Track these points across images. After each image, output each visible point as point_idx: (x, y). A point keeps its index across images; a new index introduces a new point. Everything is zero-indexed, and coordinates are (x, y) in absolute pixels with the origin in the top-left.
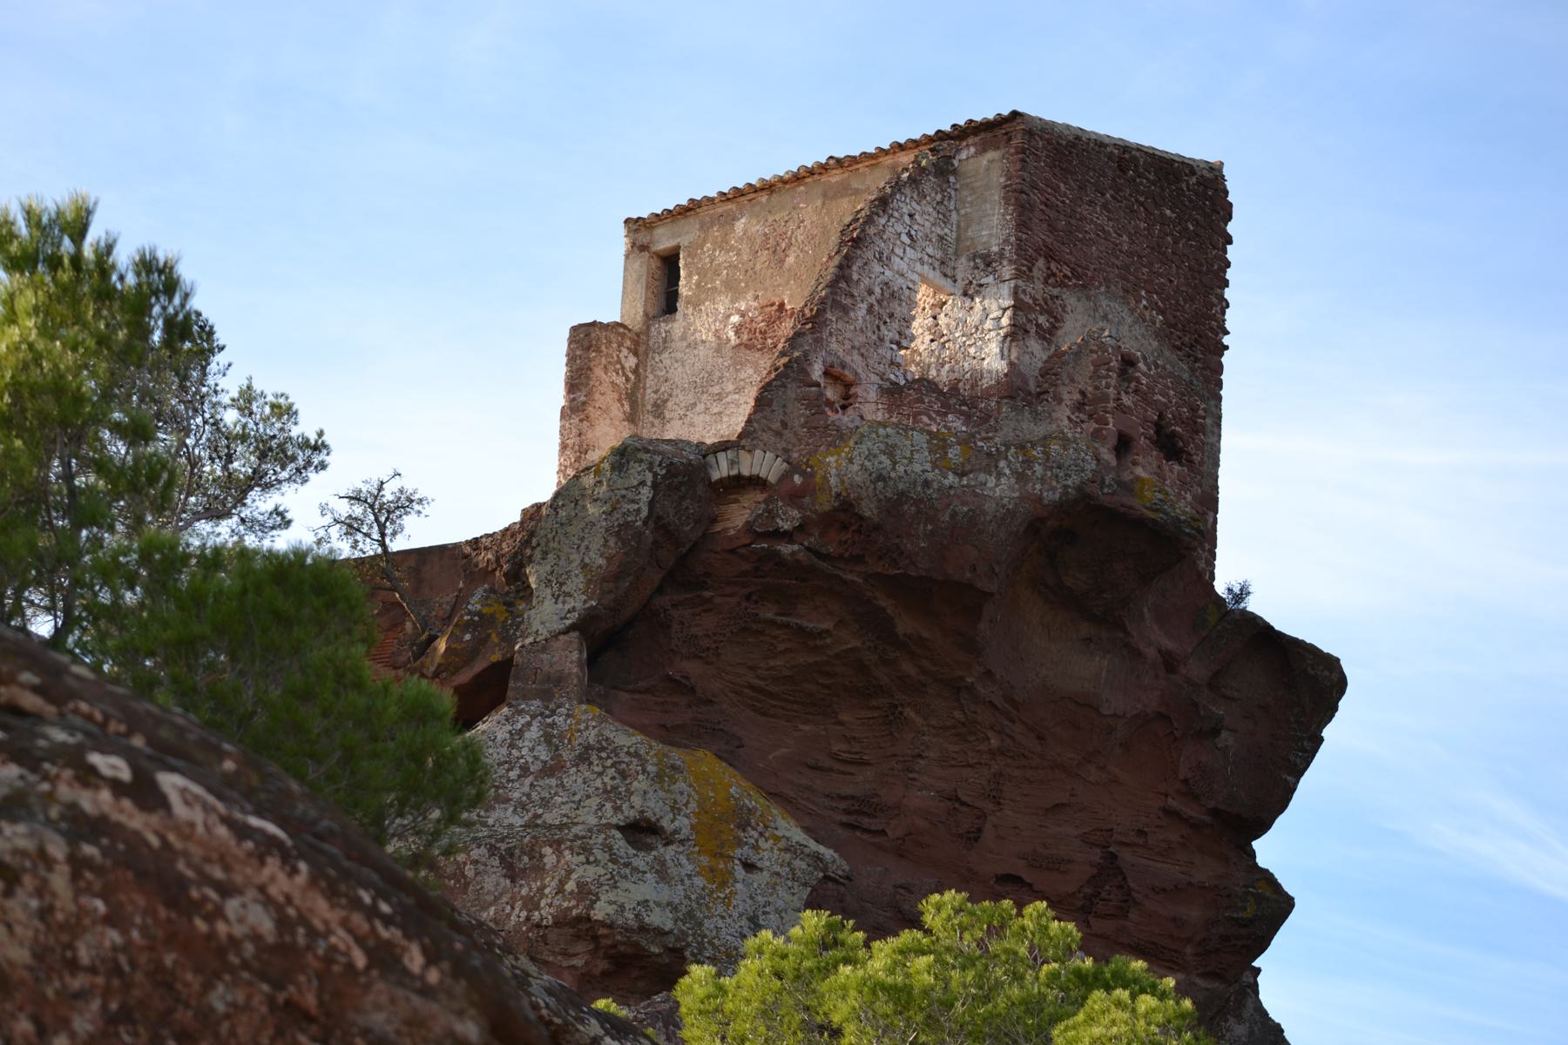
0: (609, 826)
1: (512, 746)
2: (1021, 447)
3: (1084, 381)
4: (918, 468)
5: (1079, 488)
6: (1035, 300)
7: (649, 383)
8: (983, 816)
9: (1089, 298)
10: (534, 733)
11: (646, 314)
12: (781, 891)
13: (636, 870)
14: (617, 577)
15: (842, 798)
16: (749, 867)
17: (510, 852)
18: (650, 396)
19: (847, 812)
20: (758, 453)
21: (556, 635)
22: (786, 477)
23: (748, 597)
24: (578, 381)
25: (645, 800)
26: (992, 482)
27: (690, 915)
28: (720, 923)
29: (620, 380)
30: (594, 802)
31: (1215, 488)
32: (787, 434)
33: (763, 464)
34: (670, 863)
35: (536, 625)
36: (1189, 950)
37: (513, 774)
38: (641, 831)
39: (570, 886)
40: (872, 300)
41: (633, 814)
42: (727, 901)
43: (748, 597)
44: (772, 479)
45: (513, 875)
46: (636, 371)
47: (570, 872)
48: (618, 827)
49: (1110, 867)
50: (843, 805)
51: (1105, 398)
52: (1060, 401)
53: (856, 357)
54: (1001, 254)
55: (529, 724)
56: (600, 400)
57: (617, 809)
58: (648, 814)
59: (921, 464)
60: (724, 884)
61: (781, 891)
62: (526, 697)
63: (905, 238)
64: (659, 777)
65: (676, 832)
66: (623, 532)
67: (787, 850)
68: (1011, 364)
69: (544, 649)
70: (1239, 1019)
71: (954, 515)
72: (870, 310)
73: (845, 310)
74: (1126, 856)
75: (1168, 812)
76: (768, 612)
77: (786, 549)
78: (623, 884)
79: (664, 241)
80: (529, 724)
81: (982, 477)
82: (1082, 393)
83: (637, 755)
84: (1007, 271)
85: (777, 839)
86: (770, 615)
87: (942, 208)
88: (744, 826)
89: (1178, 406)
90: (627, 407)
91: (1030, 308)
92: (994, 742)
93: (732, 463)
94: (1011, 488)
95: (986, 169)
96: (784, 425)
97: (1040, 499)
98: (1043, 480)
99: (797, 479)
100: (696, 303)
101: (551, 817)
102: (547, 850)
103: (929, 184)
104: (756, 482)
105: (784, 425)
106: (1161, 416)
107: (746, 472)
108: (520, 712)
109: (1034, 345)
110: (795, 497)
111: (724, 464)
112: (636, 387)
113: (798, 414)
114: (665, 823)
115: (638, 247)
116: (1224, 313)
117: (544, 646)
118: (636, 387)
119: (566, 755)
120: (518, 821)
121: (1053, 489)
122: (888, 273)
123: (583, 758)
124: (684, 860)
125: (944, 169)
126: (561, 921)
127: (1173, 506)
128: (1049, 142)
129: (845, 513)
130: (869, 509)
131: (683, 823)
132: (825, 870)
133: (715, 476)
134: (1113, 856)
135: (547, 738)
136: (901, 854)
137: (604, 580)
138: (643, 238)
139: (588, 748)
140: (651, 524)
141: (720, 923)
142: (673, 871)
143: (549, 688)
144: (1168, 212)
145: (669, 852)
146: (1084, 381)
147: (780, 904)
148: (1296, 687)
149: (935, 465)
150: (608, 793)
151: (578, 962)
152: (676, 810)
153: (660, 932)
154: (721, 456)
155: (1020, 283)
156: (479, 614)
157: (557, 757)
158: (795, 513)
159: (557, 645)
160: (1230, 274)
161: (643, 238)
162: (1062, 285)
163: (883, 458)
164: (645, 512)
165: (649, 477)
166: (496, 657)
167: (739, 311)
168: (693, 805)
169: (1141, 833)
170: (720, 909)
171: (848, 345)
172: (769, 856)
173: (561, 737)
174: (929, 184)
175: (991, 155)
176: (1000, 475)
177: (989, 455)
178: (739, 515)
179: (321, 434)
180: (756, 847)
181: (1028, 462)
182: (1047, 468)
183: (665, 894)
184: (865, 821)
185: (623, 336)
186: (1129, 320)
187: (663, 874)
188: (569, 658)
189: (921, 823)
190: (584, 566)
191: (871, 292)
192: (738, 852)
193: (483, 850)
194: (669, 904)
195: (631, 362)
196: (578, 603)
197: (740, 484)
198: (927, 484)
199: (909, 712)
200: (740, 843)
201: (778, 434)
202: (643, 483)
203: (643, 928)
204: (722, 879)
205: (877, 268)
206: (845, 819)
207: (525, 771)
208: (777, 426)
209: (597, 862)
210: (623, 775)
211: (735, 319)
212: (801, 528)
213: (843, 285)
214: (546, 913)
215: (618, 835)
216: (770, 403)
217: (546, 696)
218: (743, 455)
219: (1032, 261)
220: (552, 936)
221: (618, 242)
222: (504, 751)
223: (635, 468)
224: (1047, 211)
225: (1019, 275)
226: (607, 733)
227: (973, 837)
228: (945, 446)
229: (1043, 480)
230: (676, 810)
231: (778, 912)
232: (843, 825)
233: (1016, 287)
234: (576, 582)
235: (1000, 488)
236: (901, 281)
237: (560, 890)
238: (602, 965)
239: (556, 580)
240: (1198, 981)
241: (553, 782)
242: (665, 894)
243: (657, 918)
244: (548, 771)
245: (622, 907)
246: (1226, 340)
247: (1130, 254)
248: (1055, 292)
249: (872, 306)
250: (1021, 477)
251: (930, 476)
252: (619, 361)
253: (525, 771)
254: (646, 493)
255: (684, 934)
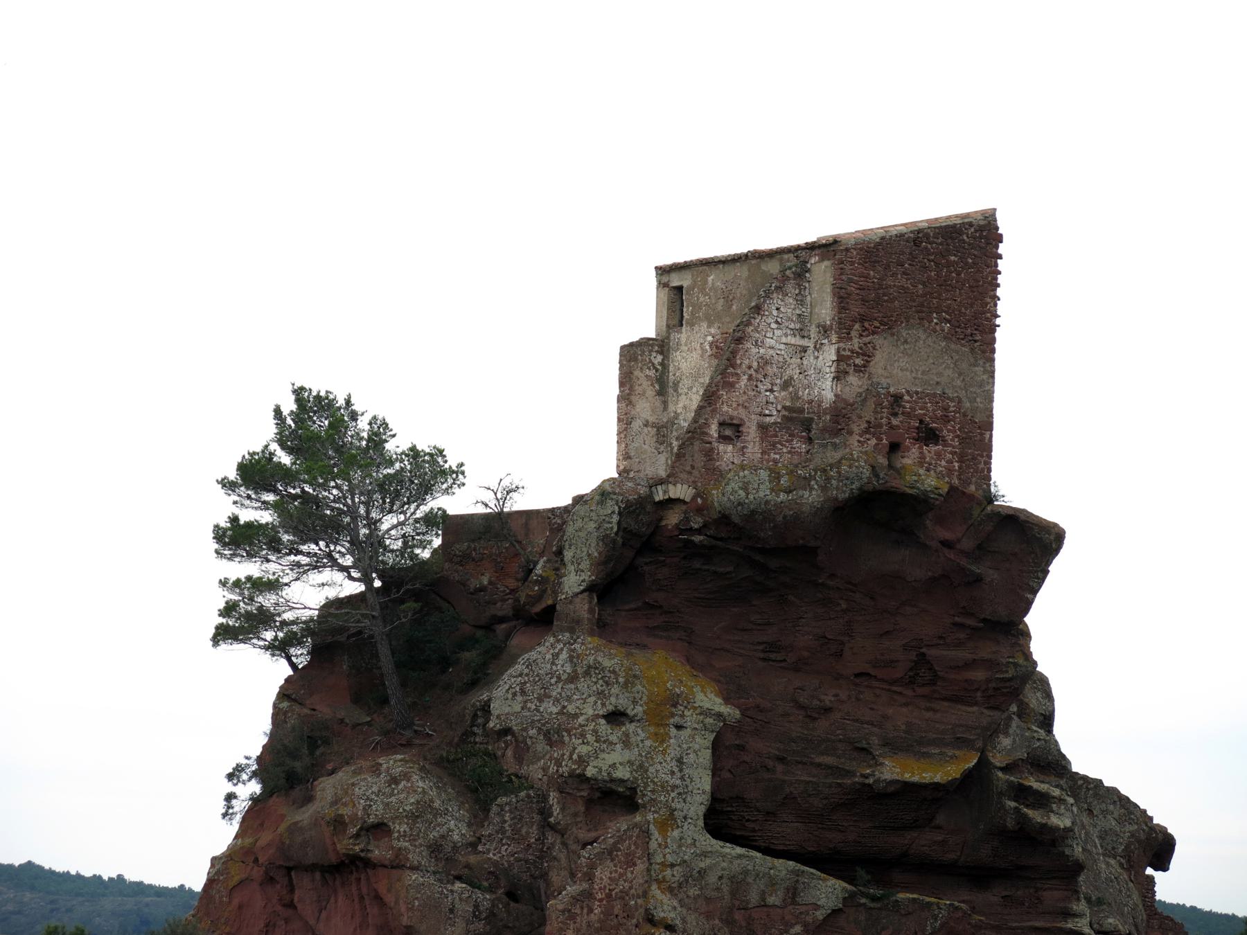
0: (597, 716)
1: (553, 663)
2: (824, 471)
3: (868, 414)
4: (761, 494)
5: (859, 489)
6: (852, 351)
7: (671, 369)
8: (843, 643)
9: (893, 335)
10: (564, 655)
11: (668, 326)
12: (698, 739)
13: (611, 743)
14: (605, 563)
15: (759, 643)
16: (679, 727)
17: (548, 732)
18: (671, 377)
19: (763, 651)
20: (679, 486)
21: (577, 595)
22: (694, 498)
23: (685, 558)
24: (626, 380)
25: (618, 699)
26: (806, 494)
27: (641, 766)
28: (659, 767)
29: (652, 373)
30: (592, 699)
31: (991, 416)
32: (695, 472)
33: (680, 491)
34: (631, 735)
35: (566, 589)
36: (979, 694)
37: (553, 681)
38: (616, 717)
39: (575, 757)
40: (752, 372)
41: (611, 708)
42: (664, 752)
43: (685, 558)
44: (687, 499)
45: (551, 743)
46: (662, 364)
47: (575, 749)
48: (604, 717)
49: (922, 659)
50: (761, 647)
51: (880, 426)
52: (850, 433)
53: (741, 410)
54: (831, 325)
55: (562, 649)
56: (638, 389)
57: (603, 705)
58: (620, 707)
59: (764, 492)
60: (663, 741)
61: (698, 739)
62: (562, 630)
63: (774, 326)
64: (626, 683)
65: (635, 715)
66: (604, 538)
67: (701, 714)
68: (836, 396)
69: (571, 602)
70: (1007, 734)
71: (785, 517)
72: (750, 378)
73: (732, 385)
74: (932, 653)
75: (955, 624)
76: (697, 564)
77: (697, 538)
78: (602, 756)
79: (684, 280)
80: (562, 649)
81: (801, 493)
82: (868, 422)
83: (614, 672)
84: (834, 338)
85: (695, 708)
86: (698, 566)
87: (799, 298)
88: (675, 706)
89: (934, 411)
90: (657, 387)
91: (849, 357)
92: (844, 606)
93: (665, 492)
94: (818, 496)
95: (822, 272)
96: (693, 467)
97: (836, 499)
98: (837, 488)
99: (699, 500)
100: (691, 324)
101: (571, 709)
102: (565, 734)
103: (791, 287)
104: (678, 501)
105: (693, 467)
106: (921, 422)
107: (672, 496)
108: (558, 641)
109: (853, 379)
110: (699, 510)
111: (661, 493)
112: (663, 373)
113: (699, 460)
114: (629, 711)
115: (662, 285)
116: (996, 305)
117: (570, 601)
118: (663, 373)
119: (580, 670)
120: (555, 710)
121: (844, 492)
122: (762, 351)
123: (587, 673)
124: (640, 731)
125: (801, 273)
126: (572, 774)
127: (923, 484)
128: (861, 249)
129: (724, 519)
130: (736, 519)
131: (639, 709)
132: (724, 720)
133: (657, 499)
134: (924, 654)
135: (571, 658)
136: (797, 670)
137: (599, 564)
138: (665, 279)
139: (589, 667)
140: (621, 533)
141: (659, 767)
142: (633, 740)
143: (573, 626)
144: (953, 258)
145: (631, 727)
146: (868, 414)
147: (697, 747)
148: (1031, 545)
149: (772, 490)
150: (600, 694)
151: (585, 794)
152: (635, 702)
153: (622, 781)
154: (659, 487)
155: (841, 345)
156: (540, 576)
157: (575, 671)
158: (700, 520)
159: (577, 600)
160: (1000, 279)
161: (665, 279)
162: (874, 333)
163: (741, 492)
164: (615, 529)
165: (616, 508)
166: (550, 602)
167: (711, 334)
168: (645, 698)
169: (941, 638)
170: (660, 758)
171: (734, 405)
172: (691, 718)
173: (578, 657)
174: (791, 287)
175: (826, 263)
176: (812, 489)
177: (805, 478)
178: (673, 519)
179: (462, 465)
180: (682, 716)
181: (828, 479)
182: (839, 481)
183: (627, 755)
184: (773, 656)
185: (652, 345)
186: (923, 337)
187: (626, 743)
188: (583, 608)
189: (806, 654)
190: (589, 555)
191: (750, 367)
192: (672, 721)
193: (534, 731)
194: (629, 762)
195: (660, 358)
196: (587, 576)
197: (671, 502)
198: (767, 502)
199: (791, 598)
200: (673, 715)
201: (690, 473)
202: (613, 512)
203: (612, 780)
204: (662, 739)
205: (754, 350)
206: (762, 655)
207: (559, 678)
208: (688, 468)
209: (588, 743)
210: (607, 684)
211: (710, 338)
212: (705, 526)
213: (731, 370)
214: (564, 770)
215: (603, 721)
216: (684, 455)
217: (572, 631)
218: (671, 487)
219: (850, 328)
220: (570, 781)
221: (652, 280)
222: (549, 666)
223: (610, 503)
224: (862, 292)
225: (840, 340)
226: (600, 659)
227: (839, 655)
228: (778, 477)
229: (837, 488)
230: (635, 702)
231: (695, 752)
232: (764, 659)
233: (838, 349)
234: (585, 564)
235: (812, 497)
236: (771, 352)
237: (571, 758)
238: (598, 794)
239: (577, 561)
240: (985, 711)
241: (573, 686)
242: (627, 755)
243: (622, 773)
244: (573, 678)
245: (600, 769)
246: (998, 321)
247: (924, 295)
248: (867, 339)
249: (751, 375)
250: (824, 488)
251: (769, 498)
252: (651, 361)
253: (559, 678)
254: (615, 518)
255: (636, 779)
